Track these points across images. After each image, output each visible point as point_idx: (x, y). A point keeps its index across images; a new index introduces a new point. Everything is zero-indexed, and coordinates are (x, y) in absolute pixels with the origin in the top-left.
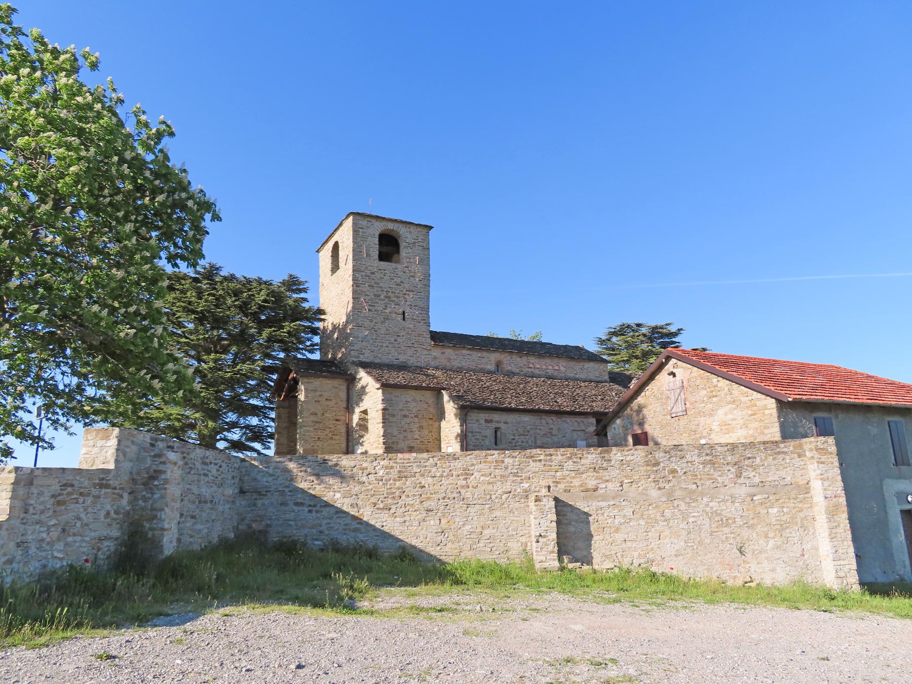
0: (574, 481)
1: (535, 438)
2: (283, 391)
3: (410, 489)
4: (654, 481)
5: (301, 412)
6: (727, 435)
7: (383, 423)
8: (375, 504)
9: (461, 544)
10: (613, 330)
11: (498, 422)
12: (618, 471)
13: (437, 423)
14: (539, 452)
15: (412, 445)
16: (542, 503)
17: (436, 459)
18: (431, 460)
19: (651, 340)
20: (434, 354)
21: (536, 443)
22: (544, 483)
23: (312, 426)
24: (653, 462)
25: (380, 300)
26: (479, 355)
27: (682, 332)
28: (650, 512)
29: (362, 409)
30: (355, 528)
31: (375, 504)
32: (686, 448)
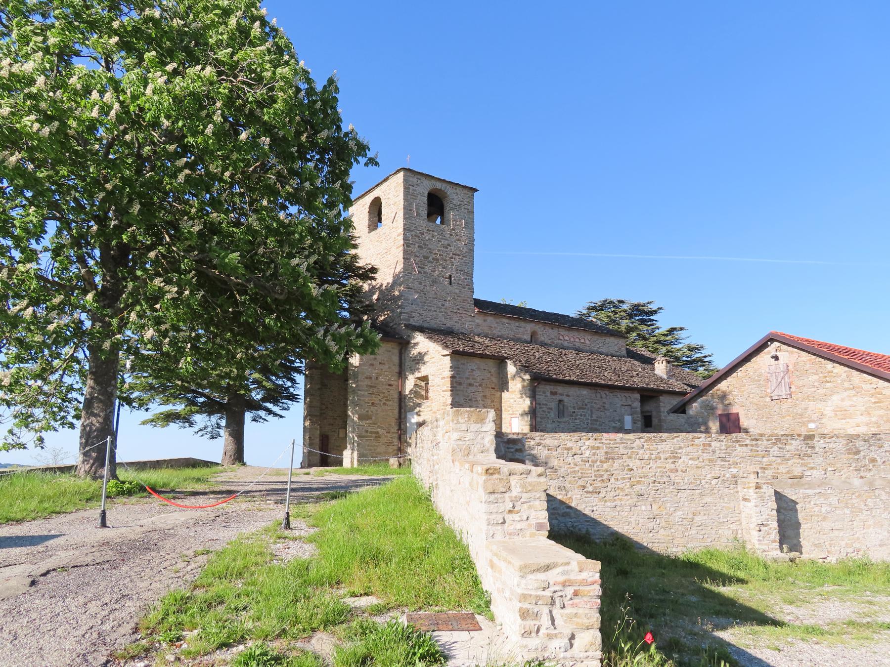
0: (780, 467)
1: (591, 411)
3: (618, 472)
4: (856, 470)
6: (844, 421)
8: (584, 487)
9: (673, 531)
10: (593, 305)
11: (561, 394)
12: (822, 459)
13: (499, 393)
14: (745, 437)
16: (762, 490)
17: (642, 440)
18: (638, 441)
19: (631, 316)
20: (477, 321)
21: (592, 417)
22: (752, 468)
23: (367, 390)
24: (854, 450)
25: (429, 262)
26: (517, 324)
27: (661, 311)
28: (854, 501)
30: (565, 512)
31: (584, 487)
32: (883, 436)
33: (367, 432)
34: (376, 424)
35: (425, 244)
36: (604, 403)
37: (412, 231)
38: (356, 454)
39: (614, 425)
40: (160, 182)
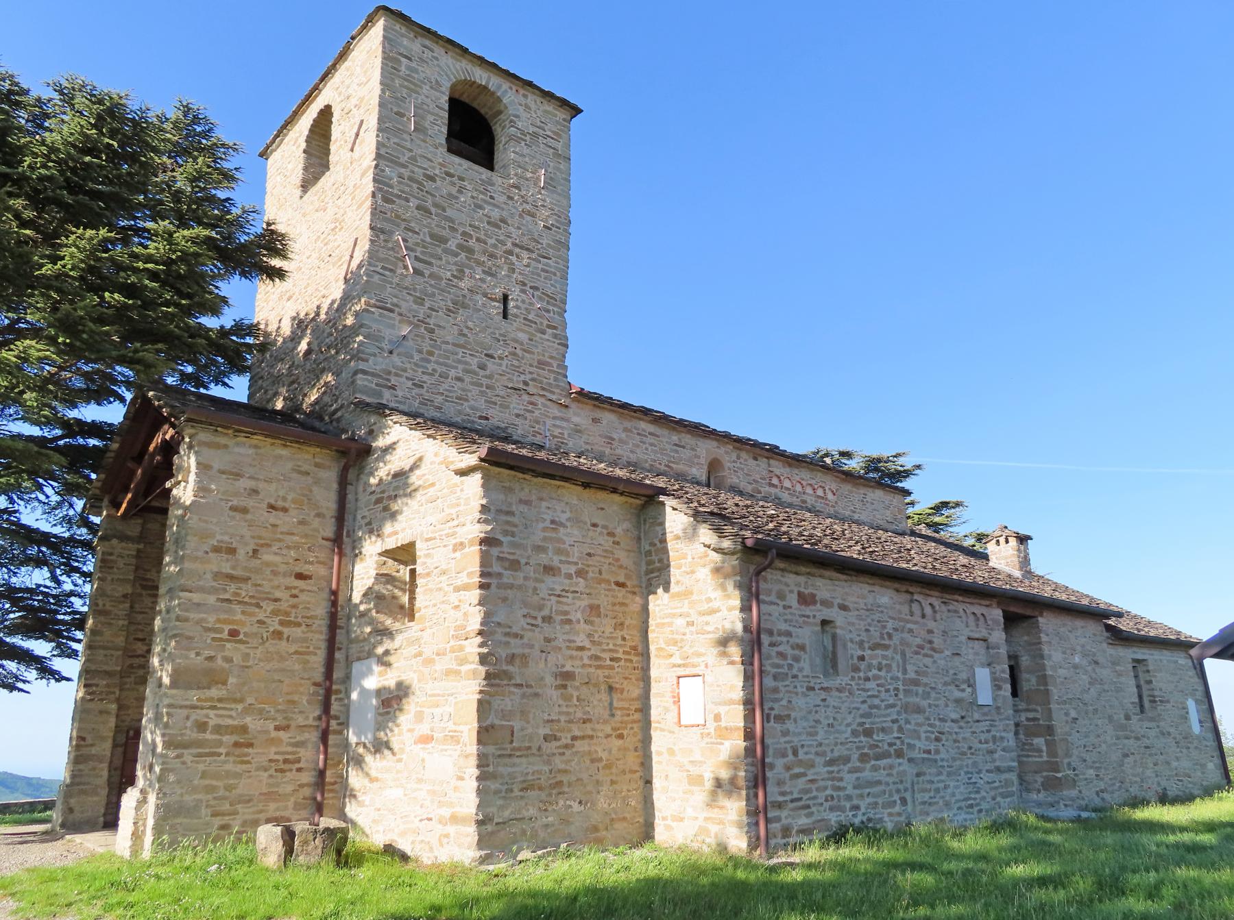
1: (903, 654)
2: (126, 490)
5: (177, 542)
7: (482, 586)
11: (826, 603)
13: (638, 599)
15: (568, 668)
20: (576, 419)
21: (905, 671)
23: (214, 591)
25: (446, 251)
26: (675, 438)
27: (917, 472)
29: (391, 543)
33: (202, 726)
34: (241, 700)
36: (930, 632)
39: (958, 694)
40: (125, 338)
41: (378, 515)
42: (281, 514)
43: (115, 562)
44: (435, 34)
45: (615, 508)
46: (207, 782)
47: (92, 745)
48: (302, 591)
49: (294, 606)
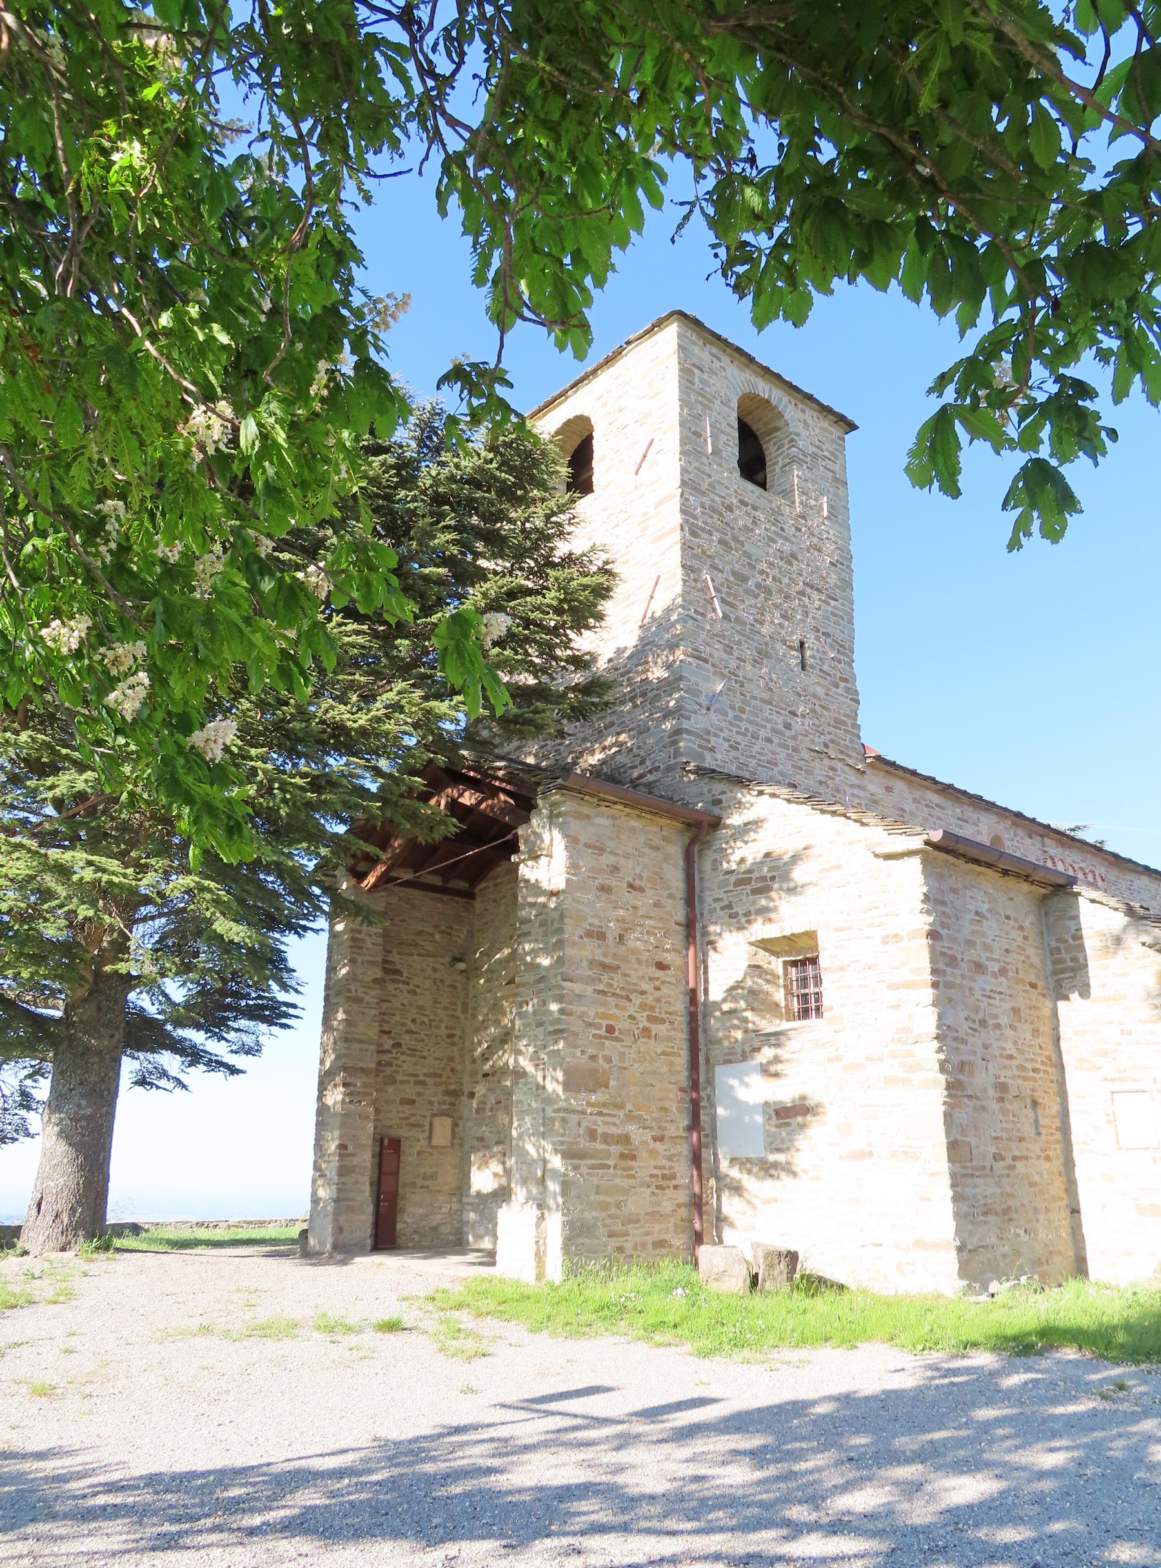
20: (872, 788)
23: (590, 980)
33: (592, 1134)
34: (620, 1107)
35: (735, 539)
37: (703, 493)
38: (555, 1223)
41: (744, 898)
42: (638, 894)
43: (363, 940)
44: (725, 342)
45: (1021, 898)
46: (601, 1198)
47: (353, 1155)
48: (663, 982)
49: (658, 1000)
